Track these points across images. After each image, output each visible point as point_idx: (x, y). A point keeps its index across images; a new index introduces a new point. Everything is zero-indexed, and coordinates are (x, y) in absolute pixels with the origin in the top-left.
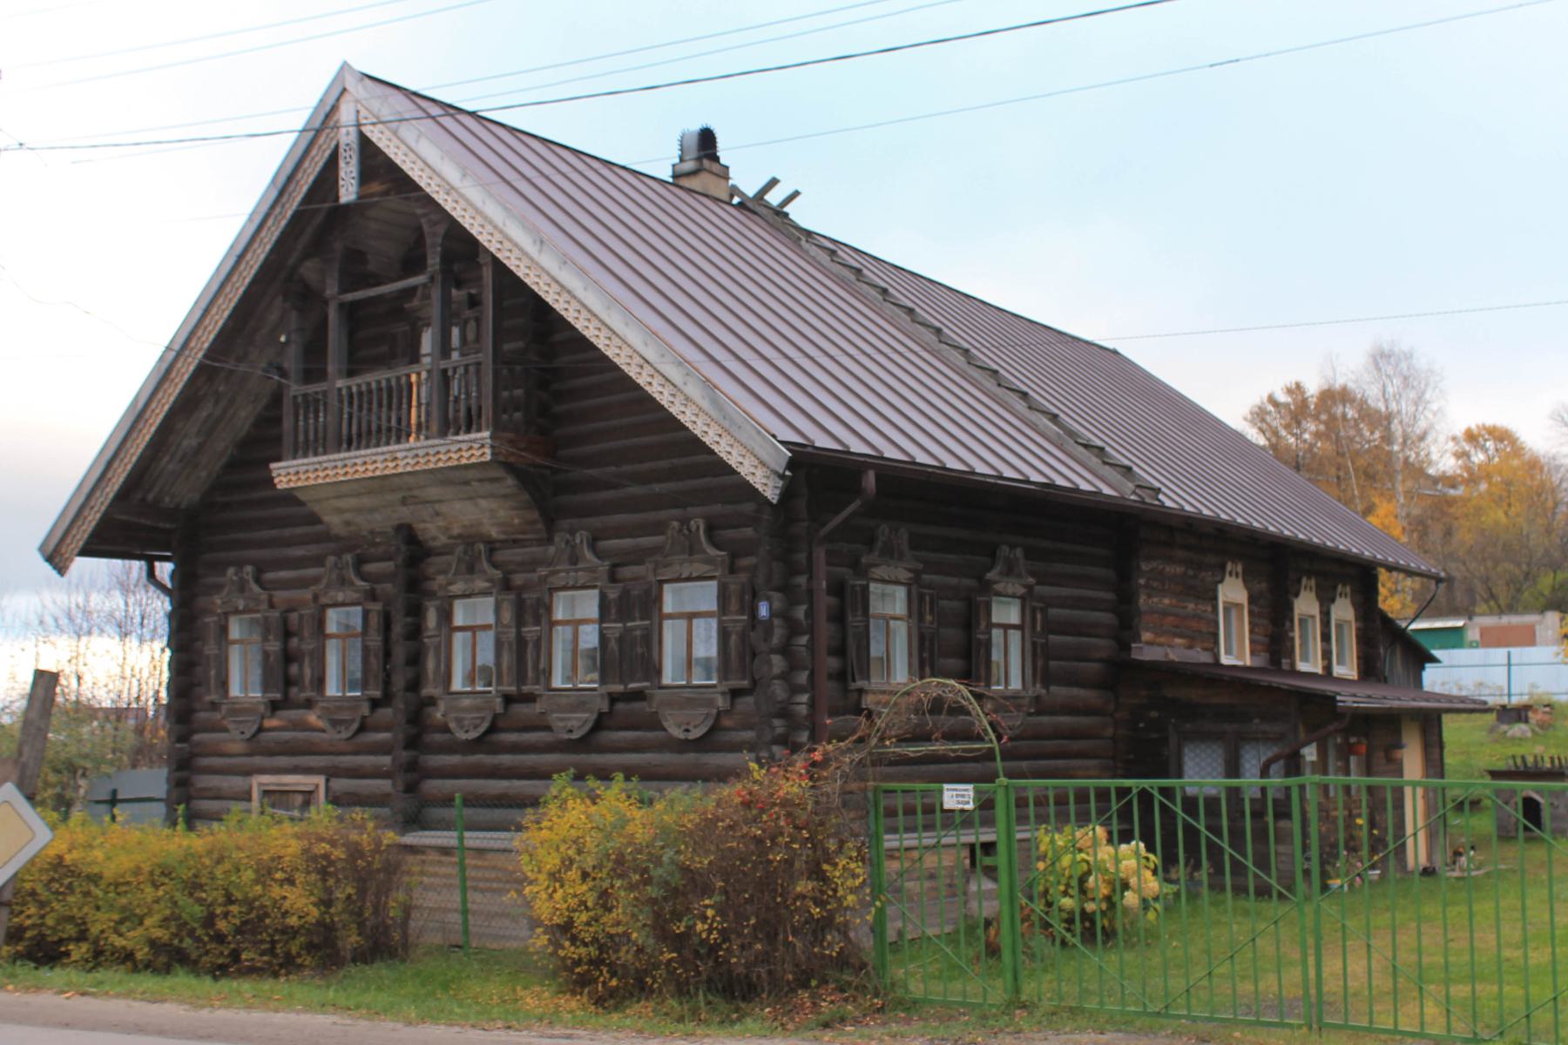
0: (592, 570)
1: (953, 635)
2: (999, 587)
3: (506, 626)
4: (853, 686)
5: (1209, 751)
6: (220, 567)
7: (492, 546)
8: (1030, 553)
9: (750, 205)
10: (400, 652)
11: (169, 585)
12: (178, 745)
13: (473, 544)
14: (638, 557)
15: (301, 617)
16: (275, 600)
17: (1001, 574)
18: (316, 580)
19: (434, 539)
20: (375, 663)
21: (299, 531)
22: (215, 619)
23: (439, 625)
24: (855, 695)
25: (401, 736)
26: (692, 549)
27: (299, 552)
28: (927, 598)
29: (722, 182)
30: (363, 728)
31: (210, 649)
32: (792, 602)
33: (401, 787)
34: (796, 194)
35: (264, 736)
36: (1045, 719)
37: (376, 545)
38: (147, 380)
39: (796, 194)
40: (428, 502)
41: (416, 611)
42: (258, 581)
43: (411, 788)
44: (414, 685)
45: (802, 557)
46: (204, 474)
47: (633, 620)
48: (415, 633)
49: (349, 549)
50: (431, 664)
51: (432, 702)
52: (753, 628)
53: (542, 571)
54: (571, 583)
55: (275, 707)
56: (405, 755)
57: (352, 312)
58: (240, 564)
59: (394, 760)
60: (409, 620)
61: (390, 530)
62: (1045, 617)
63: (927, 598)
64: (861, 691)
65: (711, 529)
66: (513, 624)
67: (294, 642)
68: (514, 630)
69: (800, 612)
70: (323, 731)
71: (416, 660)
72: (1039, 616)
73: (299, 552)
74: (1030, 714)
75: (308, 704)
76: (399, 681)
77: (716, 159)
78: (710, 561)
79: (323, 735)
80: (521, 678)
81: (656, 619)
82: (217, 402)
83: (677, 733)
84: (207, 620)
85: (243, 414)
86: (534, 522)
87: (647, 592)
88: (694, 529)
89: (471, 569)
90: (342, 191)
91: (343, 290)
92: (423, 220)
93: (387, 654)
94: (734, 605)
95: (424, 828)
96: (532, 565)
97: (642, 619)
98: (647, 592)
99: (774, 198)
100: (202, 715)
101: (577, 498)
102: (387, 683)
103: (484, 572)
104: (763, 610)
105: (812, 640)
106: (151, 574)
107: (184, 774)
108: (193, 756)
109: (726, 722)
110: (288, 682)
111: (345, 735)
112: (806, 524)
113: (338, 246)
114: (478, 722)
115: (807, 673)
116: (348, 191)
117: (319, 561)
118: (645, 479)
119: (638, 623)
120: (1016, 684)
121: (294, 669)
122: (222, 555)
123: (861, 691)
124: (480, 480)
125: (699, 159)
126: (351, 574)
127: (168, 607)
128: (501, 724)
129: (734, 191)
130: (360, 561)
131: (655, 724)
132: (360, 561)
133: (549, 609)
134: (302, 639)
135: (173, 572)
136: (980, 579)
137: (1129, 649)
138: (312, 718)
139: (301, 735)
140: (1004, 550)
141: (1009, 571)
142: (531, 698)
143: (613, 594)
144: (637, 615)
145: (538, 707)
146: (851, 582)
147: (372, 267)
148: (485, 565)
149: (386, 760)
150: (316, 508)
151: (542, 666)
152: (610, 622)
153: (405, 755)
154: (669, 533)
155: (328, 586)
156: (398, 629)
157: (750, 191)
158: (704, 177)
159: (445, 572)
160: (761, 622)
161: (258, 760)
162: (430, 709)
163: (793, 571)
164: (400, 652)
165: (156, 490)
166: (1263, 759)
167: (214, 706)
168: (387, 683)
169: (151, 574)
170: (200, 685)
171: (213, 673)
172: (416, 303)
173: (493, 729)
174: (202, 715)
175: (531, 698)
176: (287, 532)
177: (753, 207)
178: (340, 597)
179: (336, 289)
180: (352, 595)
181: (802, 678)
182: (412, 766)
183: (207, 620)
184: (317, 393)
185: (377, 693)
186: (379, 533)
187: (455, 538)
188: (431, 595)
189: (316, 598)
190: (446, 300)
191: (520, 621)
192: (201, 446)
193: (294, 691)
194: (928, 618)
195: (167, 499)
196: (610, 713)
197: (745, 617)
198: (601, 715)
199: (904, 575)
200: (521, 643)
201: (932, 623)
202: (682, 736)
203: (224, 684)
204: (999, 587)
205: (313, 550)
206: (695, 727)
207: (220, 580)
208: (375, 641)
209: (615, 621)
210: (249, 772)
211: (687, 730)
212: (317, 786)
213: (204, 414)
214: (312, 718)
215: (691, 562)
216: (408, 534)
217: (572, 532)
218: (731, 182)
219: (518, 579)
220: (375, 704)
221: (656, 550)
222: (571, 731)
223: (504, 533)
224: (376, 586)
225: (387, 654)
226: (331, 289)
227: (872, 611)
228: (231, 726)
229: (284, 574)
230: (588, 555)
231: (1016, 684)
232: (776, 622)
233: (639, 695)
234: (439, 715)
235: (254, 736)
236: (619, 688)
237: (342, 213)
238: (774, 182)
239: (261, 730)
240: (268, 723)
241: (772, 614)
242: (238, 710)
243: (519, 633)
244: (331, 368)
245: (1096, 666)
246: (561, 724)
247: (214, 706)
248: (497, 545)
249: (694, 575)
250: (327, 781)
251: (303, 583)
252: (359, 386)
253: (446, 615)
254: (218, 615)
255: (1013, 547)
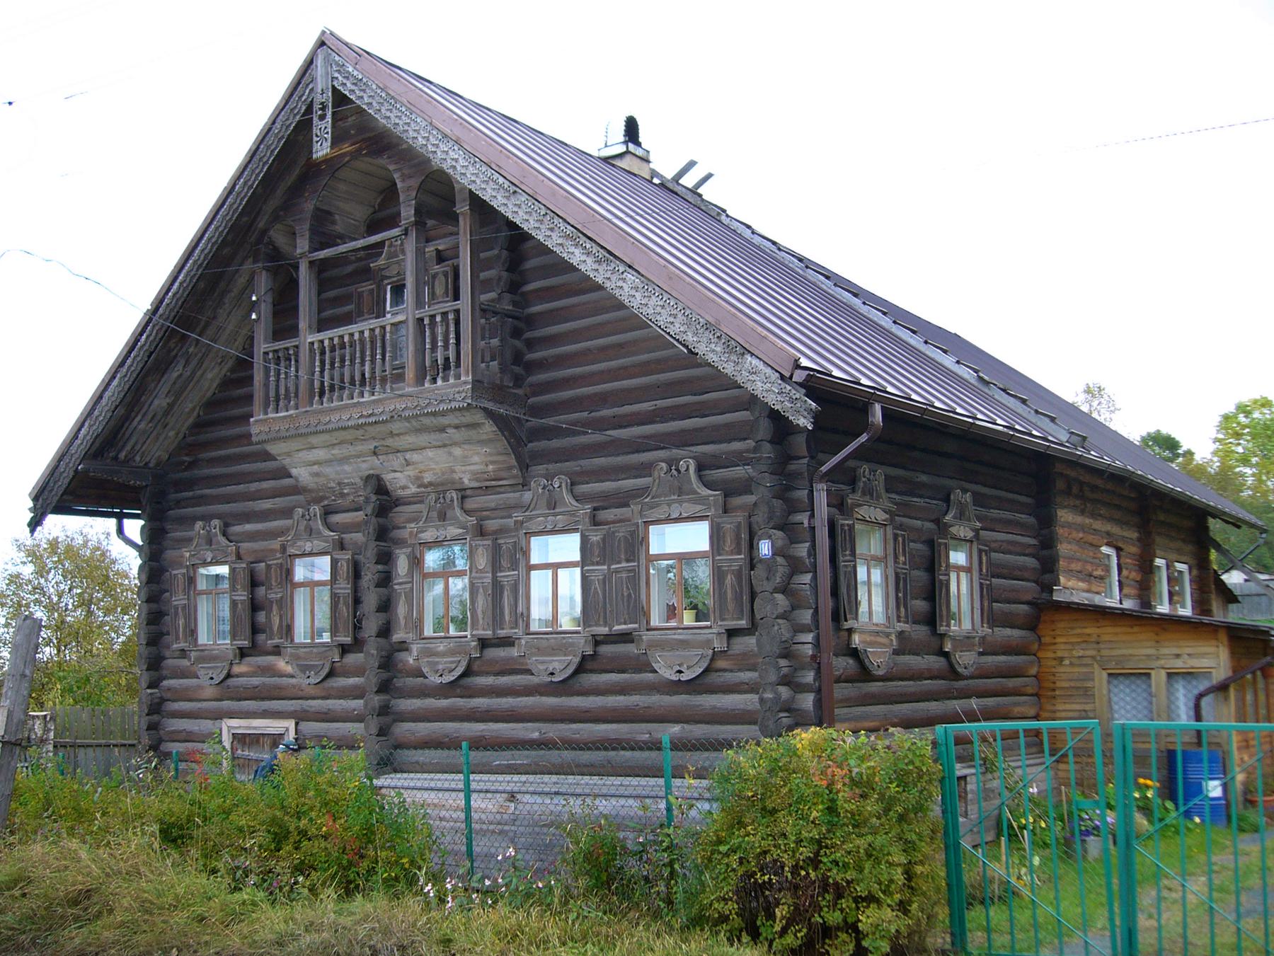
0: (572, 514)
1: (920, 575)
2: (954, 530)
3: (481, 571)
4: (847, 625)
5: (1133, 687)
6: (189, 521)
7: (464, 494)
8: (979, 500)
9: (670, 186)
10: (371, 599)
11: (140, 543)
12: (149, 691)
13: (445, 492)
14: (622, 500)
15: (268, 567)
16: (242, 552)
17: (954, 517)
18: (282, 532)
19: (404, 488)
20: (345, 611)
21: (266, 485)
22: (184, 571)
23: (410, 573)
24: (846, 634)
25: (374, 680)
26: (681, 490)
27: (266, 505)
28: (900, 539)
29: (645, 164)
30: (331, 674)
31: (178, 600)
32: (793, 540)
33: (374, 731)
34: (709, 176)
35: (231, 681)
36: (990, 659)
37: (343, 495)
38: (98, 398)
39: (709, 176)
40: (398, 451)
41: (385, 558)
42: (224, 534)
43: (383, 732)
44: (385, 632)
45: (803, 494)
46: (172, 434)
47: (619, 562)
48: (385, 580)
49: (317, 501)
50: (401, 610)
51: (403, 646)
52: (752, 567)
53: (518, 516)
54: (549, 527)
55: (243, 653)
56: (377, 700)
57: (320, 267)
58: (207, 518)
59: (366, 705)
60: (380, 567)
61: (358, 480)
62: (989, 560)
63: (900, 539)
64: (850, 631)
65: (700, 468)
66: (489, 569)
67: (261, 591)
68: (490, 575)
69: (802, 550)
70: (292, 677)
71: (386, 606)
72: (984, 558)
73: (266, 505)
74: (981, 654)
75: (277, 651)
76: (371, 626)
77: (638, 144)
78: (701, 500)
79: (293, 681)
80: (497, 620)
81: (643, 561)
82: (187, 363)
83: (669, 674)
84: (175, 572)
85: (210, 376)
86: (510, 468)
87: (633, 534)
88: (683, 470)
89: (443, 517)
90: (316, 147)
91: (314, 249)
92: (396, 176)
93: (357, 601)
94: (729, 544)
95: (395, 771)
96: (510, 508)
97: (628, 561)
98: (633, 534)
99: (689, 181)
100: (170, 662)
101: (556, 443)
102: (357, 627)
103: (455, 518)
104: (765, 548)
105: (815, 578)
106: (120, 531)
107: (155, 718)
108: (163, 700)
109: (721, 664)
110: (255, 630)
111: (313, 680)
112: (805, 461)
113: (309, 206)
114: (453, 666)
115: (811, 611)
116: (322, 149)
117: (287, 513)
118: (601, 425)
119: (624, 564)
120: (967, 625)
121: (261, 617)
122: (189, 511)
123: (850, 631)
124: (457, 427)
125: (626, 143)
126: (319, 524)
127: (139, 562)
128: (475, 667)
129: (654, 173)
130: (327, 512)
131: (644, 665)
132: (327, 512)
133: (526, 553)
134: (269, 588)
135: (143, 528)
136: (937, 521)
137: (1051, 591)
138: (282, 664)
139: (267, 680)
140: (957, 495)
141: (961, 516)
142: (508, 642)
143: (595, 538)
144: (623, 557)
145: (514, 652)
146: (842, 522)
147: (339, 228)
148: (458, 512)
149: (357, 704)
150: (287, 462)
151: (520, 609)
152: (593, 564)
153: (377, 700)
154: (656, 474)
155: (297, 537)
156: (368, 578)
157: (669, 174)
158: (628, 158)
159: (416, 520)
160: (761, 561)
161: (226, 704)
162: (402, 655)
163: (793, 508)
164: (371, 599)
165: (128, 447)
166: (1196, 692)
167: (183, 653)
168: (357, 627)
169: (120, 531)
170: (168, 634)
171: (181, 622)
172: (381, 262)
173: (467, 673)
174: (170, 662)
175: (508, 642)
176: (254, 486)
177: (669, 188)
178: (308, 547)
179: (307, 248)
180: (318, 544)
181: (806, 616)
182: (384, 710)
183: (175, 572)
184: (287, 349)
185: (348, 640)
186: (348, 484)
187: (426, 487)
188: (401, 543)
189: (283, 548)
190: (420, 252)
191: (495, 566)
192: (171, 406)
193: (261, 638)
194: (902, 558)
195: (138, 458)
196: (594, 656)
197: (742, 556)
198: (584, 658)
199: (881, 516)
200: (497, 587)
201: (904, 563)
202: (675, 677)
203: (193, 633)
204: (954, 530)
205: (279, 502)
206: (689, 668)
207: (190, 533)
208: (345, 588)
209: (598, 564)
210: (219, 716)
211: (680, 672)
212: (287, 730)
213: (175, 375)
214: (282, 664)
215: (680, 502)
216: (379, 487)
217: (550, 477)
218: (652, 166)
219: (492, 525)
220: (344, 650)
221: (644, 491)
222: (552, 674)
223: (477, 480)
224: (343, 536)
225: (357, 601)
226: (303, 245)
227: (857, 552)
228: (201, 673)
229: (248, 527)
230: (568, 498)
231: (967, 625)
232: (779, 559)
233: (626, 638)
234: (411, 661)
235: (222, 682)
236: (604, 630)
237: (313, 170)
238: (691, 164)
239: (229, 676)
240: (237, 669)
241: (776, 552)
242: (207, 657)
243: (494, 578)
244: (303, 324)
245: (1025, 607)
246: (542, 667)
247: (183, 653)
248: (468, 492)
249: (685, 515)
250: (297, 724)
251: (273, 535)
252: (331, 339)
253: (417, 562)
254: (187, 566)
255: (965, 491)
